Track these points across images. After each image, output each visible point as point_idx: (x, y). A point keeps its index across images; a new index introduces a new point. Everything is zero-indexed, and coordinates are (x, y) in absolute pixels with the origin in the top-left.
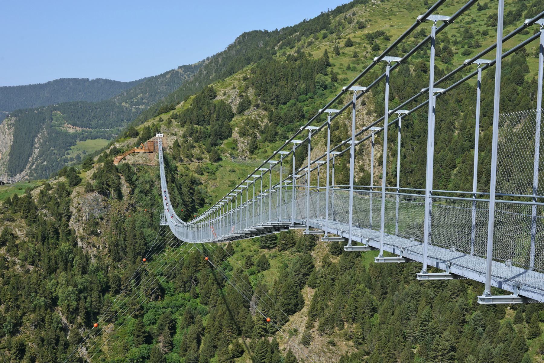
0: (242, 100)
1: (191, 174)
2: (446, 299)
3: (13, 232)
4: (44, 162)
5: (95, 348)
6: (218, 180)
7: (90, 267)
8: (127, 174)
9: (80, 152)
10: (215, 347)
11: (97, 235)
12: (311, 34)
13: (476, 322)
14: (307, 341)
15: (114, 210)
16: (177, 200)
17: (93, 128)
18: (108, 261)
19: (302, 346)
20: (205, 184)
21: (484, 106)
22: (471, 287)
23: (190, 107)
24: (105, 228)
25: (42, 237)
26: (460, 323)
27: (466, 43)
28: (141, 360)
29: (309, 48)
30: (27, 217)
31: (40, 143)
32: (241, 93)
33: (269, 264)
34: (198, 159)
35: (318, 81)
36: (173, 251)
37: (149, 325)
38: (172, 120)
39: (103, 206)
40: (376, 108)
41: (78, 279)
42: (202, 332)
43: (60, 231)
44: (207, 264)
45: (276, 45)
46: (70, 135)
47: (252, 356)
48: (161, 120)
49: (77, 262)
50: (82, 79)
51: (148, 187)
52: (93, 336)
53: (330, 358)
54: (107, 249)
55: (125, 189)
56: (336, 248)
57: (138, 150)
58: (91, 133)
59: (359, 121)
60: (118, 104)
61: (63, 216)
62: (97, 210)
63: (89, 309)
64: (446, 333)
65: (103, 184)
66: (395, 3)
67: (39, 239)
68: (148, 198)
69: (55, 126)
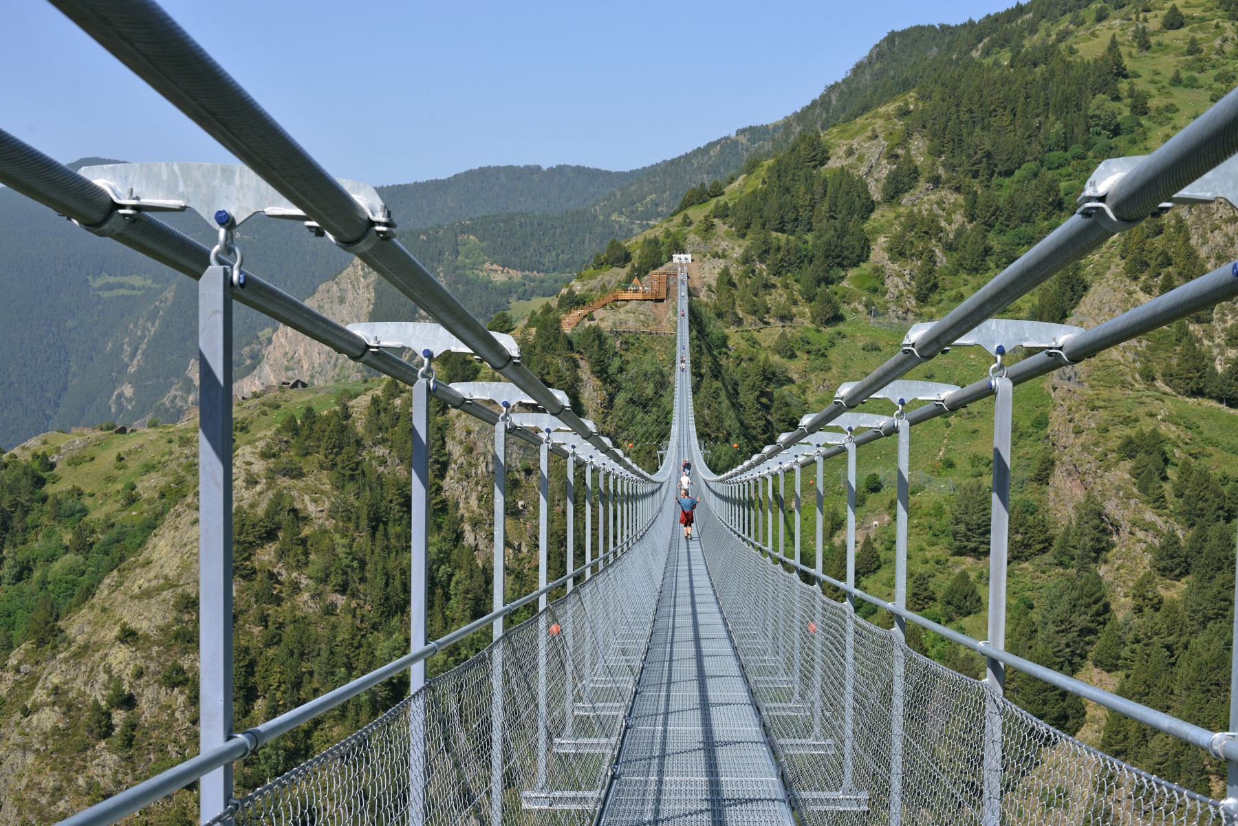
0: (894, 167)
1: (762, 357)
6: (834, 371)
8: (595, 356)
12: (1065, 13)
16: (727, 423)
17: (546, 271)
20: (799, 382)
25: (370, 520)
34: (783, 318)
35: (1098, 112)
38: (716, 221)
48: (687, 222)
49: (461, 587)
50: (527, 167)
51: (649, 390)
56: (1172, 557)
57: (627, 296)
59: (1221, 210)
60: (601, 218)
62: (515, 448)
67: (364, 523)
68: (649, 418)
69: (464, 267)
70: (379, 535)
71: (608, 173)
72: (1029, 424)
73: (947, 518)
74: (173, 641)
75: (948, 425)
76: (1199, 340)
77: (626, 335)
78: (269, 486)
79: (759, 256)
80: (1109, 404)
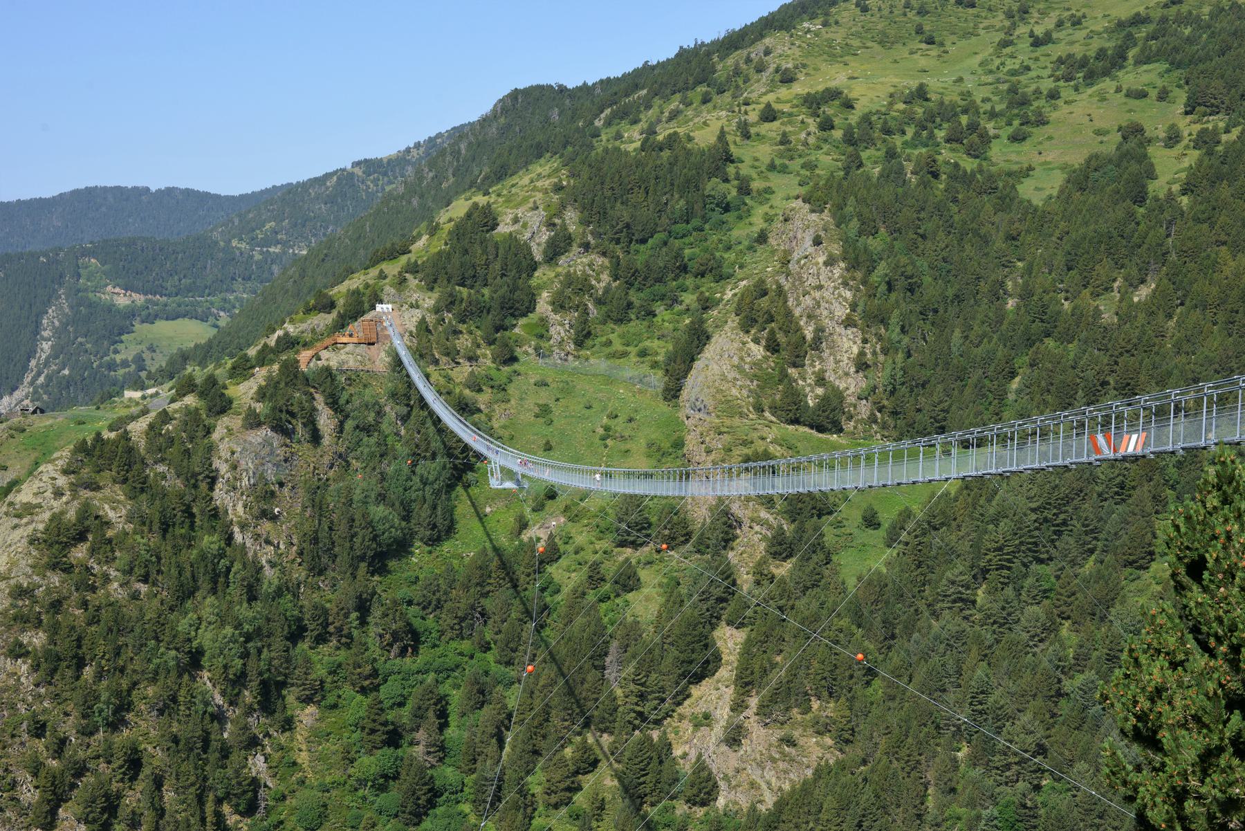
0: (553, 233)
1: (457, 390)
2: (1020, 647)
3: (101, 513)
4: (64, 369)
5: (283, 757)
6: (513, 402)
7: (265, 587)
8: (328, 390)
9: (143, 347)
10: (536, 753)
11: (274, 518)
12: (674, 93)
13: (1086, 693)
14: (734, 738)
15: (305, 466)
16: (433, 444)
17: (169, 296)
18: (299, 574)
19: (724, 748)
20: (486, 411)
21: (1069, 249)
22: (1067, 624)
23: (443, 247)
24: (291, 505)
25: (162, 524)
26: (1052, 696)
27: (1017, 115)
28: (381, 781)
29: (673, 123)
30: (125, 481)
31: (54, 327)
32: (551, 219)
33: (639, 580)
34: (470, 359)
35: (713, 193)
36: (430, 552)
37: (391, 708)
38: (407, 275)
39: (282, 458)
40: (845, 251)
41: (244, 611)
42: (506, 722)
43: (195, 510)
44: (504, 579)
45: (597, 116)
46: (118, 311)
47: (615, 771)
48: (382, 276)
49: (238, 576)
50: (135, 189)
51: (371, 417)
52: (277, 732)
53: (786, 772)
54: (295, 548)
55: (326, 420)
56: (780, 544)
57: (345, 340)
58: (166, 305)
59: (810, 279)
60: (222, 244)
61: (200, 477)
62: (270, 465)
63: (266, 676)
64: (1025, 718)
65: (281, 411)
66: (853, 29)
67: (156, 527)
68: (373, 440)
69: (86, 290)
70: (168, 536)
71: (218, 196)
72: (668, 445)
73: (611, 518)
74: (12, 622)
75: (606, 446)
76: (795, 381)
77: (349, 373)
78: (74, 497)
79: (446, 306)
80: (731, 430)
